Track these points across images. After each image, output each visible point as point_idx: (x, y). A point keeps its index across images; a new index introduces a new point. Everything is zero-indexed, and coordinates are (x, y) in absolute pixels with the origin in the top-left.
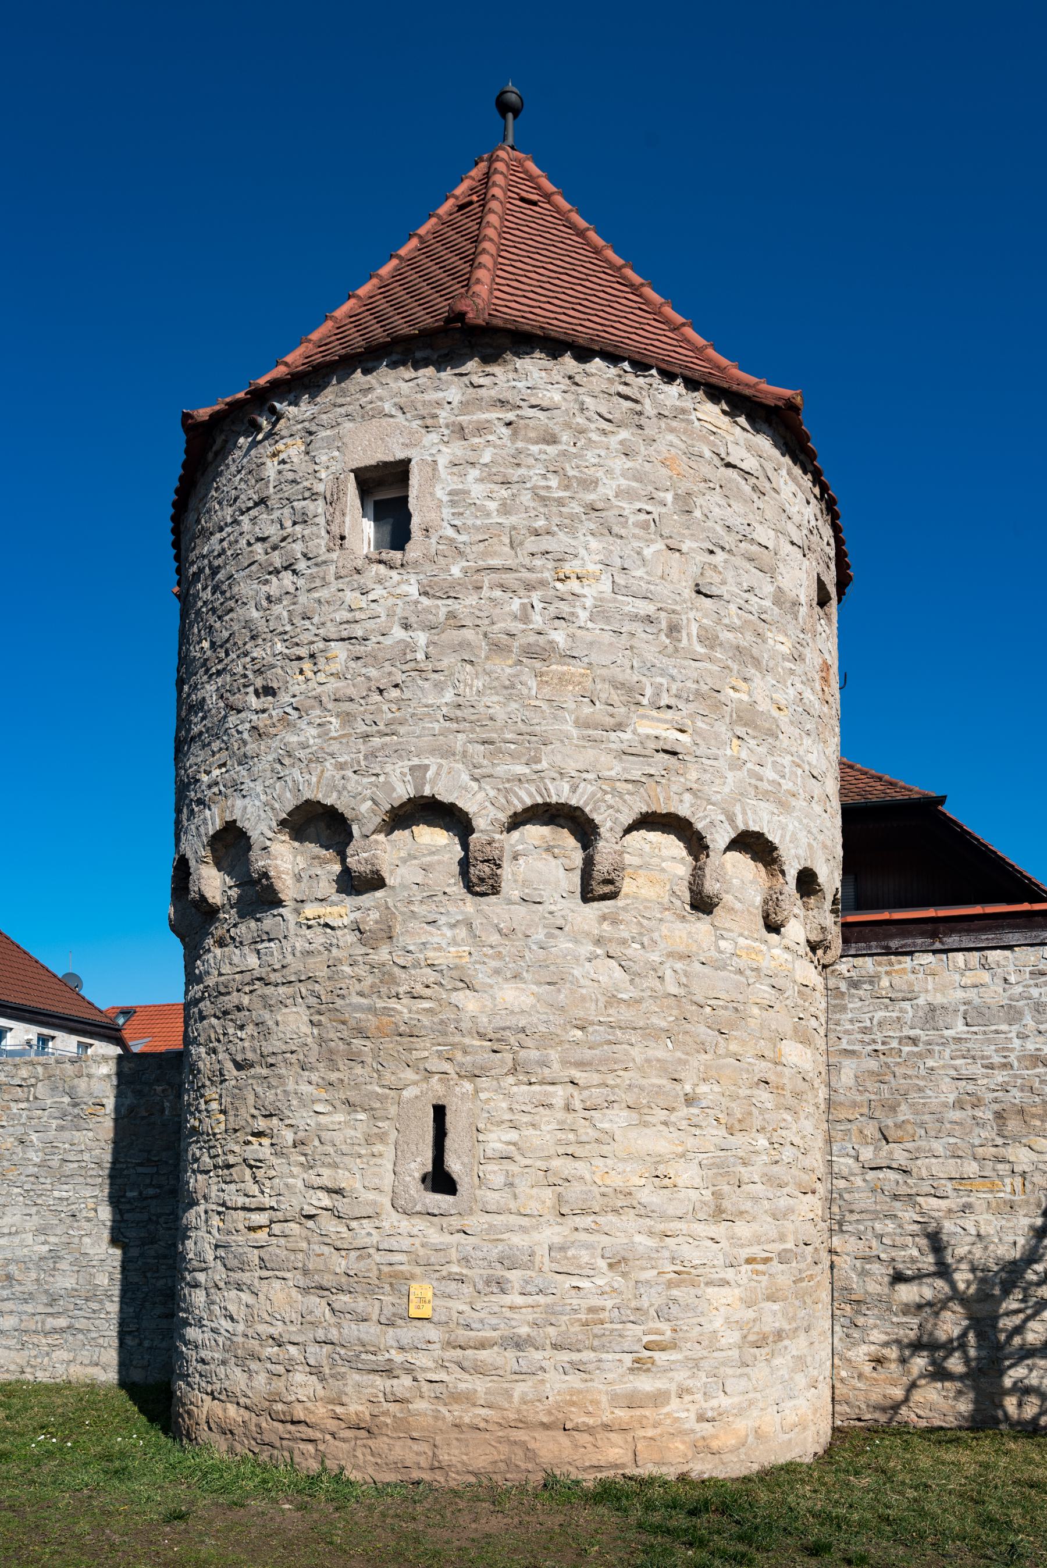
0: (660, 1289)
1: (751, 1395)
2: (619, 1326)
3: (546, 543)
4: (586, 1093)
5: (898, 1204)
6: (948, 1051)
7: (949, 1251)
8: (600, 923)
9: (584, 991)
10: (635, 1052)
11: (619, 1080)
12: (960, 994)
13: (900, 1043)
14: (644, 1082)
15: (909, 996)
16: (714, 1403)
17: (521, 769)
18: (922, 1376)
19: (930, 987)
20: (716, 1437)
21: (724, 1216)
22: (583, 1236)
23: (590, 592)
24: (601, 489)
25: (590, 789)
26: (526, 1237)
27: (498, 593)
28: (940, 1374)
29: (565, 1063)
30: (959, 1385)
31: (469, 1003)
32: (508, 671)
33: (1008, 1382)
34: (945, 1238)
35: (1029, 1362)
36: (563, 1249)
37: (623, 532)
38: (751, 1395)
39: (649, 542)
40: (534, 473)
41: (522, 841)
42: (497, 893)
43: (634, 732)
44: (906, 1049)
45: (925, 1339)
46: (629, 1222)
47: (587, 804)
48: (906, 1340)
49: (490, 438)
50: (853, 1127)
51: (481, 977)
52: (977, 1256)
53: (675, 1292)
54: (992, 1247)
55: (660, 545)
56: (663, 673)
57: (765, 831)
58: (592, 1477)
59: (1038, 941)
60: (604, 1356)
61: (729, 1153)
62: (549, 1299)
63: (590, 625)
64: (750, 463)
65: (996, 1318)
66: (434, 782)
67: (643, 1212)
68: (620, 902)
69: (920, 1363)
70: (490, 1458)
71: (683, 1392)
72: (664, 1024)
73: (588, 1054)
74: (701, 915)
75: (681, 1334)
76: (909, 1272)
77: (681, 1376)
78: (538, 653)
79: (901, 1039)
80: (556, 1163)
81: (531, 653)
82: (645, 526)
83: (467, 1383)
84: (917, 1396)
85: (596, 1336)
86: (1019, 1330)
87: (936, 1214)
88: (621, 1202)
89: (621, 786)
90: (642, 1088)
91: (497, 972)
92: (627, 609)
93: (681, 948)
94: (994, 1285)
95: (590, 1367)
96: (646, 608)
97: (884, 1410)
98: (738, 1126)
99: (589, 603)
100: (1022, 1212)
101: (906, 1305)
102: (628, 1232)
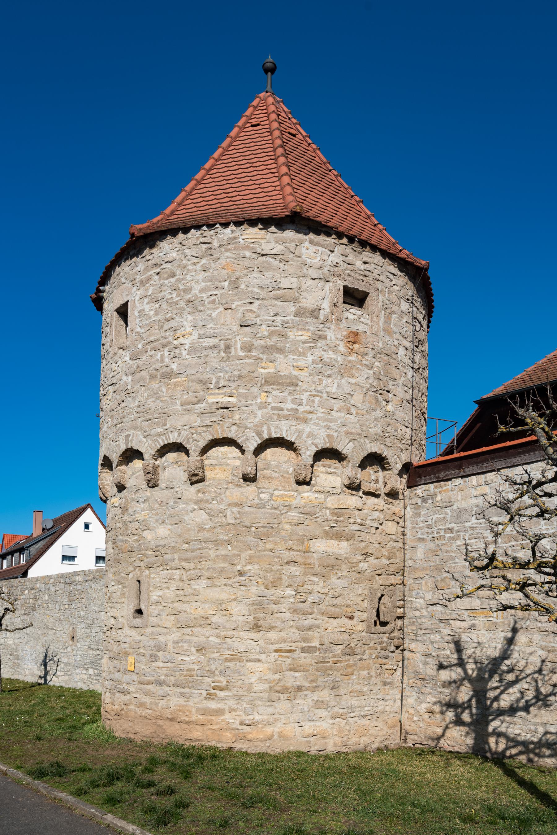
0: (220, 662)
1: (276, 716)
2: (201, 678)
3: (173, 324)
4: (189, 573)
5: (442, 625)
6: (467, 535)
7: (464, 652)
8: (197, 494)
9: (189, 526)
10: (211, 552)
11: (203, 566)
12: (474, 501)
13: (445, 532)
14: (216, 566)
15: (449, 504)
16: (251, 717)
17: (160, 430)
18: (451, 723)
19: (459, 499)
20: (251, 733)
21: (260, 629)
22: (187, 637)
23: (187, 341)
24: (193, 291)
25: (186, 433)
26: (165, 637)
27: (153, 352)
28: (459, 722)
29: (180, 560)
30: (467, 728)
31: (148, 535)
32: (157, 386)
33: (490, 729)
34: (462, 644)
35: (501, 718)
36: (177, 642)
37: (202, 309)
38: (276, 716)
39: (214, 309)
40: (166, 294)
41: (166, 461)
42: (157, 486)
43: (207, 403)
44: (447, 535)
45: (452, 701)
46: (206, 631)
47: (184, 441)
48: (444, 702)
49: (152, 282)
50: (423, 582)
51: (152, 524)
52: (478, 655)
53: (228, 664)
54: (484, 650)
55: (221, 309)
56: (222, 370)
57: (284, 436)
58: (188, 744)
59: (512, 464)
60: (193, 691)
61: (265, 598)
62: (172, 665)
63: (187, 357)
64: (278, 248)
65: (486, 691)
66: (132, 441)
67: (214, 626)
68: (206, 483)
69: (450, 715)
70: (150, 731)
71: (231, 710)
72: (226, 538)
73: (190, 555)
74: (248, 483)
75: (231, 684)
76: (445, 663)
77: (231, 703)
78: (168, 376)
79: (445, 529)
80: (176, 605)
81: (164, 376)
82: (213, 302)
83: (147, 700)
84: (448, 733)
85: (190, 682)
86: (496, 699)
87: (458, 630)
88: (205, 621)
89: (200, 429)
90: (214, 569)
91: (157, 521)
92: (204, 345)
93: (237, 501)
94: (486, 672)
95: (188, 695)
96: (214, 341)
97: (433, 739)
98: (270, 585)
99: (187, 347)
100: (500, 629)
101: (444, 682)
102: (203, 635)
